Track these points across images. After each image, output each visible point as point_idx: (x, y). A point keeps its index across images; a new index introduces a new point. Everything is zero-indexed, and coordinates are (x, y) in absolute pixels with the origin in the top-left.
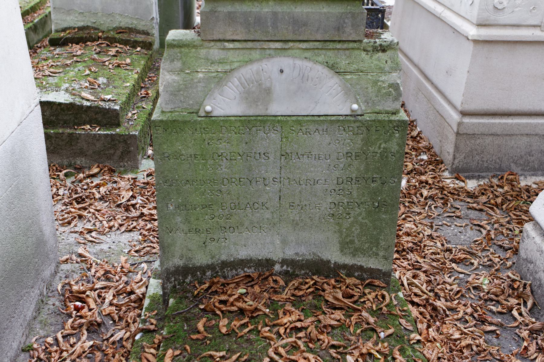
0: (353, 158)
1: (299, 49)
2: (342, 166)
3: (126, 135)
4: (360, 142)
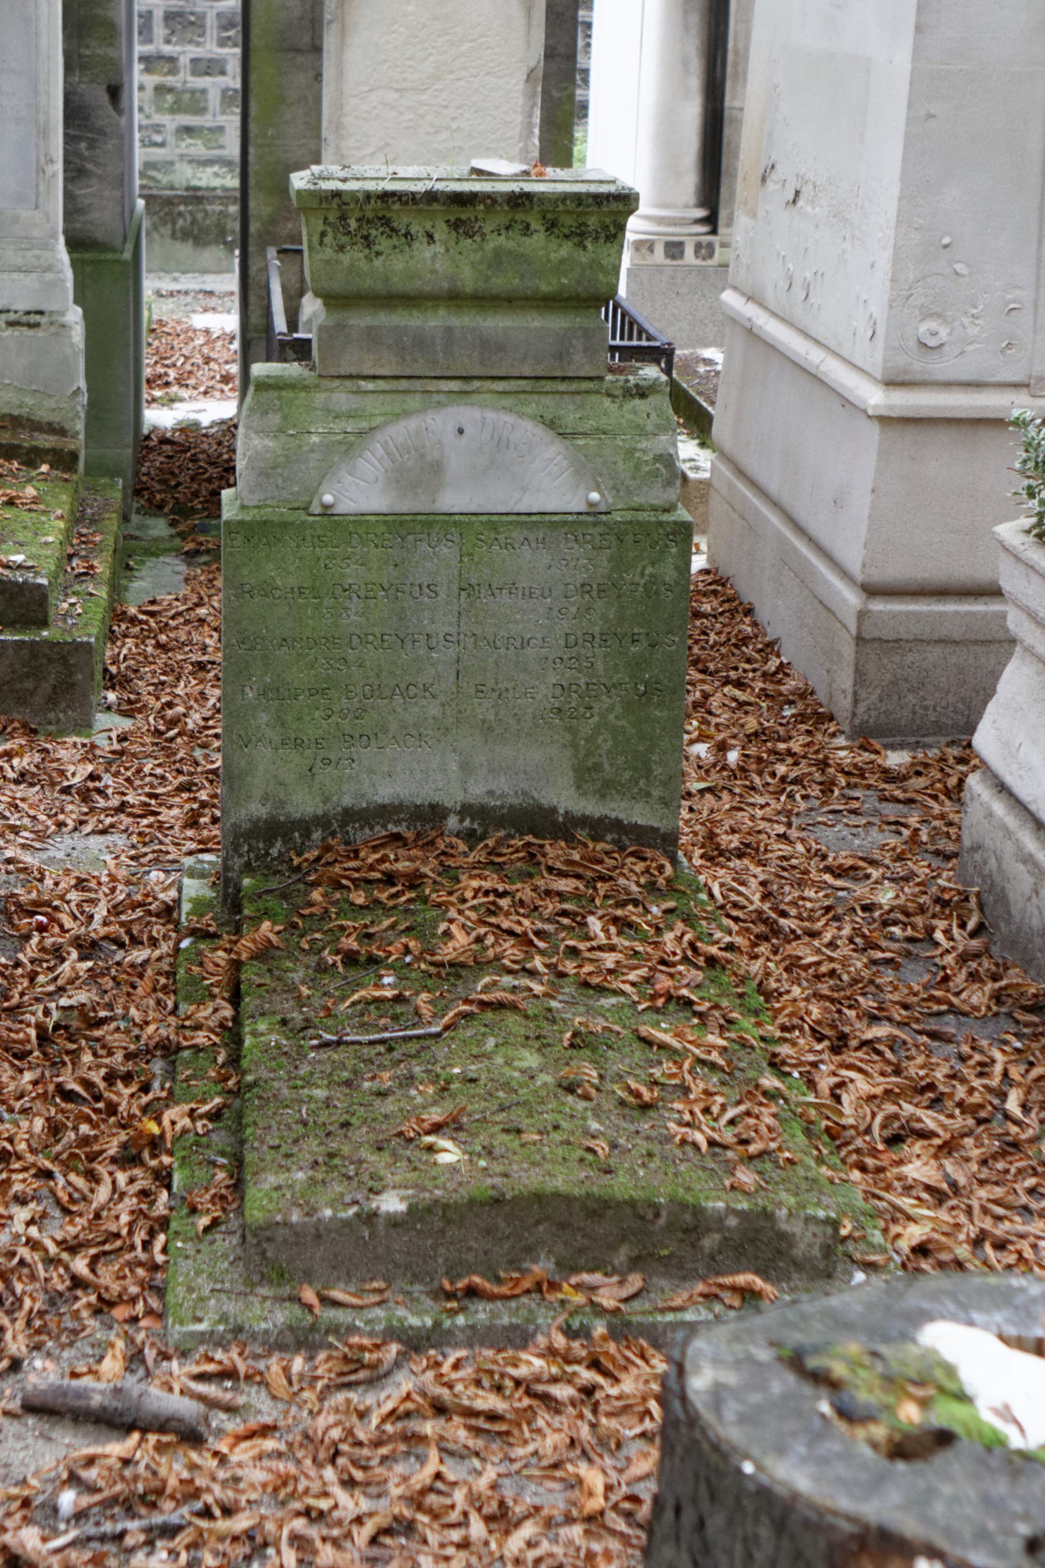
0: (595, 594)
1: (491, 392)
2: (573, 610)
3: (66, 643)
4: (605, 563)
